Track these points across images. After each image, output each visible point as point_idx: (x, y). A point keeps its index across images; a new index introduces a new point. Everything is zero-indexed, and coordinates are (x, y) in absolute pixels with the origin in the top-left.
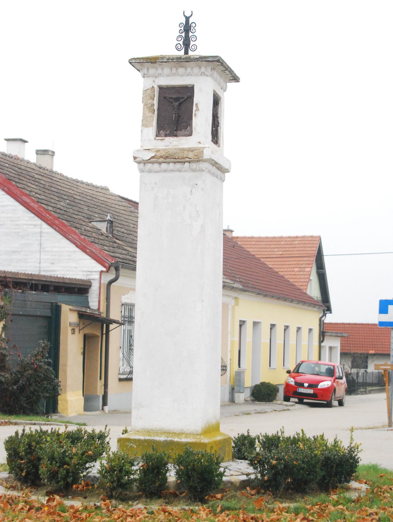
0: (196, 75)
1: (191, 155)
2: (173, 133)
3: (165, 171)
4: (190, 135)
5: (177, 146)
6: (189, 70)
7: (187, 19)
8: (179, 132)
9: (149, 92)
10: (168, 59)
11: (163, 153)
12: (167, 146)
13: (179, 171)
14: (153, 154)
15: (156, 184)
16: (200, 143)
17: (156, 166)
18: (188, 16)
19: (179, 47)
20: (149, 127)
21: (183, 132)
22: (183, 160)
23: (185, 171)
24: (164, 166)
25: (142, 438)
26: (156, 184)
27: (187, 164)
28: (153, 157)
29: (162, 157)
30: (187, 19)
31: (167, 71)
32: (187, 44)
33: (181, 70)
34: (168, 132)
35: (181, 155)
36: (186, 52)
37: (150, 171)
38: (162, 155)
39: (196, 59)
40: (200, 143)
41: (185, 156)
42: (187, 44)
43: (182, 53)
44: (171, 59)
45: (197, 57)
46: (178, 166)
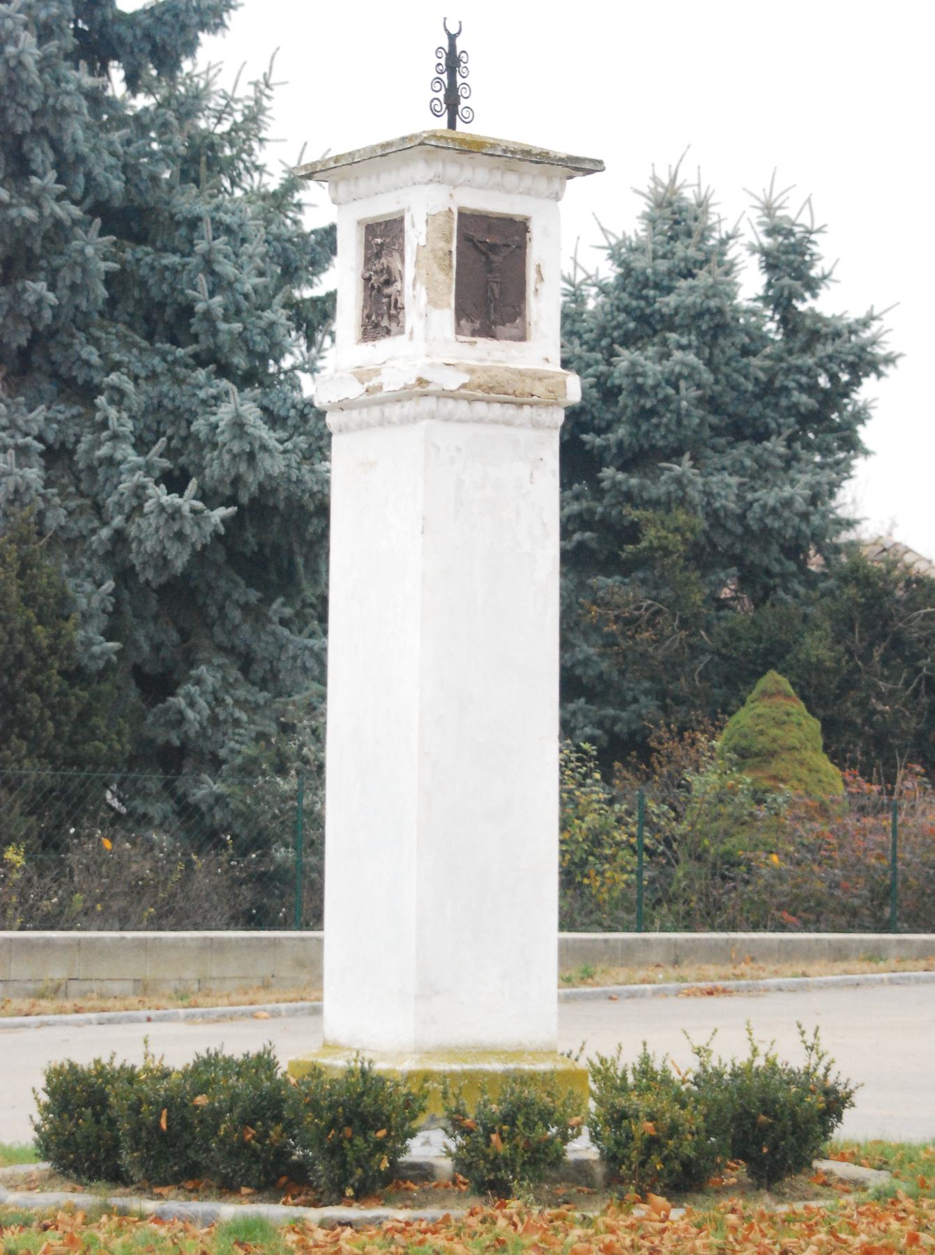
0: (538, 195)
1: (539, 389)
2: (487, 332)
3: (480, 421)
4: (522, 338)
5: (501, 362)
6: (527, 181)
7: (452, 38)
8: (500, 329)
9: (441, 219)
10: (505, 151)
11: (483, 379)
12: (481, 360)
13: (508, 423)
14: (465, 379)
15: (459, 450)
16: (547, 360)
17: (463, 407)
18: (453, 32)
19: (438, 108)
20: (441, 307)
21: (508, 329)
22: (519, 400)
23: (521, 425)
24: (480, 408)
25: (456, 1067)
26: (459, 450)
27: (527, 409)
28: (464, 386)
29: (479, 387)
30: (452, 38)
31: (481, 175)
32: (452, 101)
33: (511, 179)
34: (477, 325)
35: (519, 387)
36: (452, 125)
37: (448, 419)
38: (481, 381)
39: (561, 160)
40: (547, 360)
41: (528, 389)
42: (452, 101)
43: (442, 123)
44: (512, 152)
45: (563, 156)
46: (510, 411)
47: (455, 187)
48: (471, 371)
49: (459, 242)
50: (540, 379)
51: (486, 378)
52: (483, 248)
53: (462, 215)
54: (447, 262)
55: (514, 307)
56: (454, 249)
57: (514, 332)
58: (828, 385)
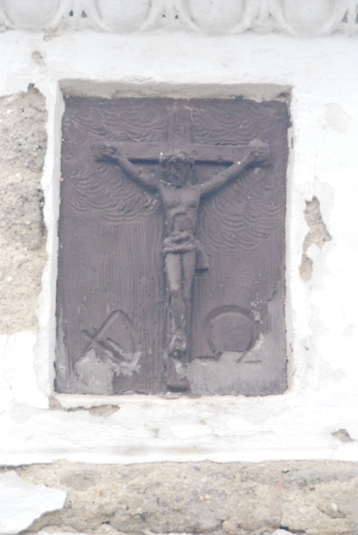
8: (200, 369)
12: (131, 450)
14: (54, 500)
34: (132, 365)
38: (110, 502)
47: (51, 33)
48: (82, 478)
49: (66, 170)
50: (303, 484)
51: (123, 492)
52: (145, 174)
53: (77, 102)
54: (31, 217)
55: (247, 312)
56: (49, 180)
57: (248, 372)
58: (151, 353)
